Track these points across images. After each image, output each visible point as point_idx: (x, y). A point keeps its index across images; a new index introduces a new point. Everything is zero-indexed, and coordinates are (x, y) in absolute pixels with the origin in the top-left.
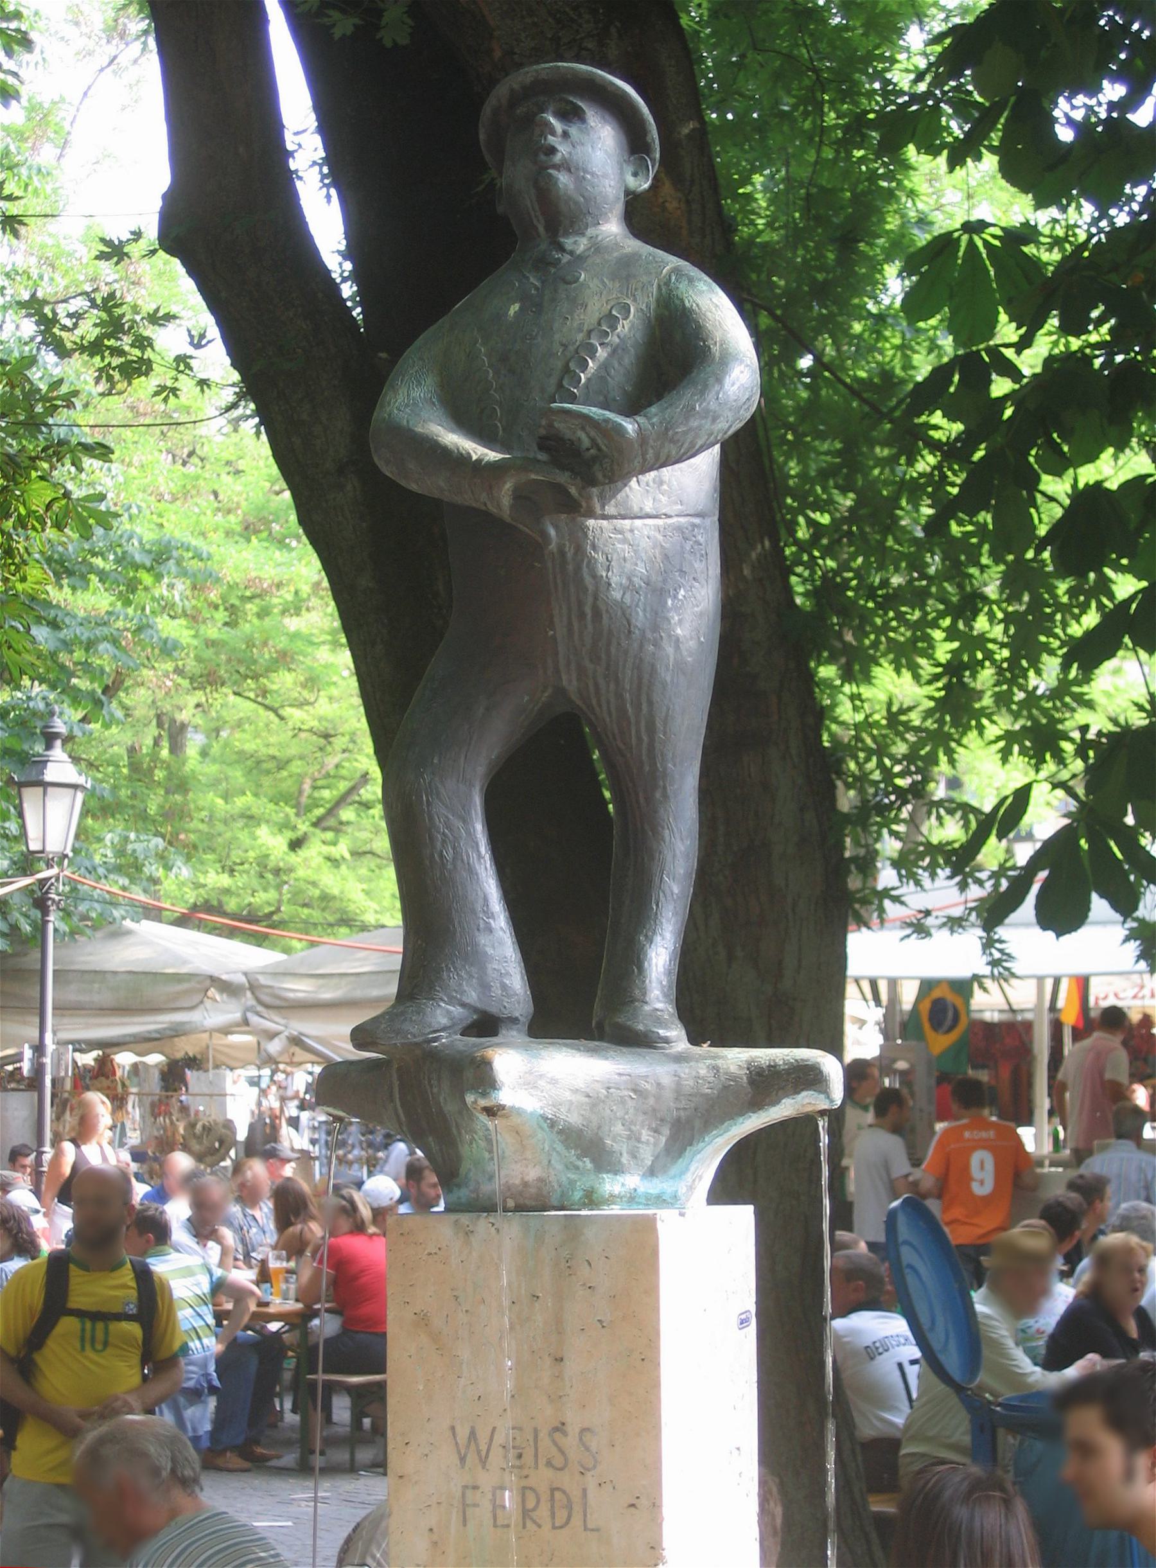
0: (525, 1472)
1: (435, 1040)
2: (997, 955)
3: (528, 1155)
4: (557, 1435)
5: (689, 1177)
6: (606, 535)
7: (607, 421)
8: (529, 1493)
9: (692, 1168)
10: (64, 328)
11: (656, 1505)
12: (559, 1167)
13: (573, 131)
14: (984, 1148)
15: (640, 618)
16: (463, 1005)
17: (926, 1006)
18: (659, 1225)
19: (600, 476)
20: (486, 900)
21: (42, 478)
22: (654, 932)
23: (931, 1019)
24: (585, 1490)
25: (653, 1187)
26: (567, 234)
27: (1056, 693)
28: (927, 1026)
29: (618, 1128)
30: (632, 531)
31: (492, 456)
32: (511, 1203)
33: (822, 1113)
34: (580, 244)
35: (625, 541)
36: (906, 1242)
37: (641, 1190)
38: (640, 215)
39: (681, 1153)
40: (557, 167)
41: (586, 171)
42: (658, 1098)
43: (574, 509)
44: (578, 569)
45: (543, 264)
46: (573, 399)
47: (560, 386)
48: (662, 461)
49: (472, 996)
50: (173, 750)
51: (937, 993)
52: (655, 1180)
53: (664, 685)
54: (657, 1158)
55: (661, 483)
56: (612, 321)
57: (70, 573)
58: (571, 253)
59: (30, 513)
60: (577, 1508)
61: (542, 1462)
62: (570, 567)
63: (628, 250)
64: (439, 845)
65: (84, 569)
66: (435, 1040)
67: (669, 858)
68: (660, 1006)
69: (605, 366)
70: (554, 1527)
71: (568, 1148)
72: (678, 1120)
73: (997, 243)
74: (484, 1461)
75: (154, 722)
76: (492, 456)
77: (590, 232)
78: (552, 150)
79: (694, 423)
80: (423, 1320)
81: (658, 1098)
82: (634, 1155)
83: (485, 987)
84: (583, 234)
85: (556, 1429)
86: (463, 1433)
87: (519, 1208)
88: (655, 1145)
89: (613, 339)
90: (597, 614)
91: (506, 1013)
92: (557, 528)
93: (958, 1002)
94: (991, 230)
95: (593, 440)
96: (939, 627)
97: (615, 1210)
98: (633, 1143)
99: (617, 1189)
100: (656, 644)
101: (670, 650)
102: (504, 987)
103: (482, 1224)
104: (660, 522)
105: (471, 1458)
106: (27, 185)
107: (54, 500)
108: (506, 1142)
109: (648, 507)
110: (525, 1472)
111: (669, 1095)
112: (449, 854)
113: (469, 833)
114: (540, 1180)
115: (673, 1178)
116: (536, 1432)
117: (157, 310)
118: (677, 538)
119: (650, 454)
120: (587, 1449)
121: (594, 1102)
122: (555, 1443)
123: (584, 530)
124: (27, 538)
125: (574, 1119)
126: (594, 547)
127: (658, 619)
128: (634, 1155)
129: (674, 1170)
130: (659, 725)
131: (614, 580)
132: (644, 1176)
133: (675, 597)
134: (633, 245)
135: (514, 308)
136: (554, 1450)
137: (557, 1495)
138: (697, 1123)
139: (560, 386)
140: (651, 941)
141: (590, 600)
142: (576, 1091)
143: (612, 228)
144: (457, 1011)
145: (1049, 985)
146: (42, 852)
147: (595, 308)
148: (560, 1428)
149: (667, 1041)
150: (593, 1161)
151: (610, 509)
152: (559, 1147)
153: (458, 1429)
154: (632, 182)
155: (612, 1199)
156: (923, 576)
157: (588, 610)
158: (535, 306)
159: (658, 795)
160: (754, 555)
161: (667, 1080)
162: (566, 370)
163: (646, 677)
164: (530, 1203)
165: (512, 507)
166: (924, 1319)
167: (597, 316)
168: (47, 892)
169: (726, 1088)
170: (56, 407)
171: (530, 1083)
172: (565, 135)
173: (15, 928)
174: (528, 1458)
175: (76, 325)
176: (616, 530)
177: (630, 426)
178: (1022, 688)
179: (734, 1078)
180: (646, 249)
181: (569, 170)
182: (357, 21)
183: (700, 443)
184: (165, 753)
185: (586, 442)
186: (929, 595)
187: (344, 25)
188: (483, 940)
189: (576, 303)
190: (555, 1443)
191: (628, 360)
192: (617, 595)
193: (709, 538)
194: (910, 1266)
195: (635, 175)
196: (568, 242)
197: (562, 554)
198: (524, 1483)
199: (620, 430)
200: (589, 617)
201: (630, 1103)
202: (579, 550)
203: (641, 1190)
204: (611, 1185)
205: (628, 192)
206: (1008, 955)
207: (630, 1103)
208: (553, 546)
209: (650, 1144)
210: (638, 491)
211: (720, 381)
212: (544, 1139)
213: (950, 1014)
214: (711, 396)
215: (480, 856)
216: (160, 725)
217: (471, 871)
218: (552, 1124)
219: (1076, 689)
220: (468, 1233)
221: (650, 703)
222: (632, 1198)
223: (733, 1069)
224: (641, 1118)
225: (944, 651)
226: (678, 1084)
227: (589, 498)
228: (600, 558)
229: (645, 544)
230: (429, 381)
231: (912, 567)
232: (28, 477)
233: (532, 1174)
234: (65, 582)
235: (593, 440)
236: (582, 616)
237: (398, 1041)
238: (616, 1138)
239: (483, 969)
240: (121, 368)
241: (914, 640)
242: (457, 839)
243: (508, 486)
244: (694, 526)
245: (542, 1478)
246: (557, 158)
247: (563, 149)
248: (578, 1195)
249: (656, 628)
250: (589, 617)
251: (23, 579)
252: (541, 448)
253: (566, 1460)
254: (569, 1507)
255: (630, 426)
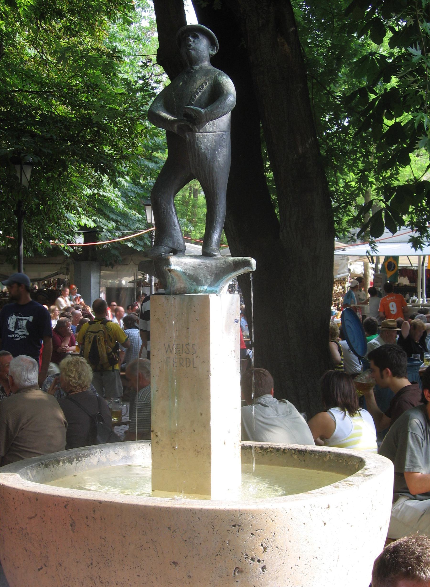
0: (180, 354)
1: (162, 255)
2: (373, 246)
3: (181, 281)
4: (187, 346)
5: (220, 287)
6: (200, 136)
7: (197, 110)
8: (181, 359)
9: (221, 285)
10: (133, 85)
11: (209, 362)
12: (188, 284)
13: (196, 41)
14: (393, 302)
15: (209, 156)
16: (168, 247)
17: (386, 264)
18: (210, 297)
19: (197, 123)
20: (174, 222)
21: (140, 124)
22: (214, 230)
23: (388, 267)
24: (193, 359)
25: (211, 289)
26: (194, 66)
27: (390, 177)
28: (386, 269)
29: (202, 275)
30: (207, 136)
31: (173, 118)
32: (178, 293)
33: (251, 272)
34: (197, 67)
35: (205, 138)
36: (347, 320)
37: (208, 290)
38: (214, 61)
39: (217, 281)
40: (191, 49)
41: (198, 50)
42: (211, 268)
43: (192, 131)
44: (194, 145)
45: (189, 73)
46: (192, 105)
47: (190, 101)
48: (211, 119)
49: (171, 245)
50: (194, 197)
51: (389, 260)
52: (211, 288)
53: (216, 172)
54: (211, 282)
55: (214, 124)
56: (203, 86)
57: (161, 149)
58: (195, 70)
59: (138, 133)
60: (191, 362)
61: (184, 352)
62: (192, 145)
63: (208, 68)
64: (163, 210)
65: (164, 148)
66: (162, 255)
67: (218, 213)
68: (215, 247)
69: (200, 97)
70: (187, 367)
71: (190, 279)
72: (216, 273)
73: (379, 58)
74: (171, 352)
75: (189, 189)
76: (173, 118)
77: (200, 65)
78: (190, 45)
79: (218, 110)
80: (158, 320)
81: (211, 268)
82: (206, 281)
83: (174, 243)
84: (198, 65)
85: (187, 344)
86: (167, 346)
87: (180, 294)
88: (211, 279)
89: (202, 90)
90: (199, 156)
91: (179, 249)
92: (189, 135)
93: (395, 263)
94: (377, 55)
95: (195, 114)
96: (360, 160)
97: (201, 294)
98: (205, 278)
99: (202, 289)
100: (213, 162)
101: (217, 164)
102: (178, 243)
103: (171, 297)
104: (214, 133)
105: (169, 351)
106: (144, 45)
107: (144, 129)
108: (176, 278)
109: (211, 130)
110: (180, 354)
111: (214, 267)
112: (165, 212)
113: (170, 207)
114: (184, 287)
115: (216, 287)
116: (183, 345)
117: (157, 80)
118: (218, 137)
119: (208, 118)
120: (194, 349)
121: (195, 268)
122: (187, 348)
123: (195, 135)
124: (138, 139)
125: (191, 273)
126: (197, 140)
127: (214, 157)
128: (206, 281)
129: (216, 285)
130: (215, 181)
131: (203, 147)
132: (208, 286)
133: (218, 151)
134: (211, 67)
135: (181, 83)
136: (187, 349)
137: (187, 359)
138: (221, 274)
139: (190, 101)
140: (214, 232)
141: (197, 152)
142: (191, 266)
143: (206, 64)
144: (167, 248)
145: (422, 257)
146: (151, 223)
147: (199, 82)
148: (188, 344)
149: (215, 255)
150: (196, 283)
151: (201, 131)
152: (188, 279)
153: (166, 345)
154: (211, 52)
155: (201, 292)
156: (356, 147)
157: (196, 154)
158: (186, 83)
159: (215, 198)
160: (309, 142)
161: (213, 264)
162: (191, 98)
163: (211, 170)
164: (182, 292)
165: (177, 131)
166: (351, 340)
167: (199, 85)
168: (152, 234)
169: (228, 266)
170: (143, 105)
171: (178, 264)
172: (194, 41)
173: (145, 244)
174: (181, 351)
175: (136, 84)
176: (203, 136)
177: (203, 111)
178: (382, 176)
179: (230, 264)
180: (214, 68)
181: (194, 50)
182: (207, 3)
183: (220, 115)
184: (192, 197)
185: (194, 115)
186: (358, 152)
187: (204, 5)
188: (173, 232)
189: (195, 82)
190: (187, 348)
191: (206, 95)
192: (203, 151)
193: (227, 137)
194: (348, 326)
195: (212, 51)
196: (194, 67)
197: (190, 141)
198: (180, 357)
199: (200, 112)
200: (197, 156)
201: (205, 269)
202: (194, 140)
203: (208, 290)
204: (201, 288)
205: (210, 55)
206: (376, 246)
207: (205, 269)
208: (188, 139)
209: (210, 279)
210: (208, 126)
211: (225, 100)
212: (184, 277)
213: (393, 266)
214: (223, 104)
215: (173, 212)
216: (190, 190)
217: (171, 216)
218: (185, 274)
219: (395, 176)
220: (168, 299)
221: (212, 176)
222: (205, 291)
223: (229, 261)
224: (207, 273)
225: (361, 165)
226: (216, 265)
227: (195, 128)
228: (199, 142)
229: (210, 139)
230: (162, 101)
231: (353, 145)
232: (137, 124)
233: (182, 286)
234: (159, 151)
235: (195, 114)
236: (195, 156)
237: (153, 255)
238: (201, 277)
239: (173, 238)
240: (148, 95)
241: (353, 164)
242: (167, 208)
243: (176, 125)
244: (223, 134)
245: (184, 356)
246: (192, 47)
247: (193, 45)
248: (193, 291)
249: (213, 158)
250: (197, 156)
251: (137, 150)
252: (184, 116)
253: (189, 352)
254: (190, 363)
255: (203, 111)
